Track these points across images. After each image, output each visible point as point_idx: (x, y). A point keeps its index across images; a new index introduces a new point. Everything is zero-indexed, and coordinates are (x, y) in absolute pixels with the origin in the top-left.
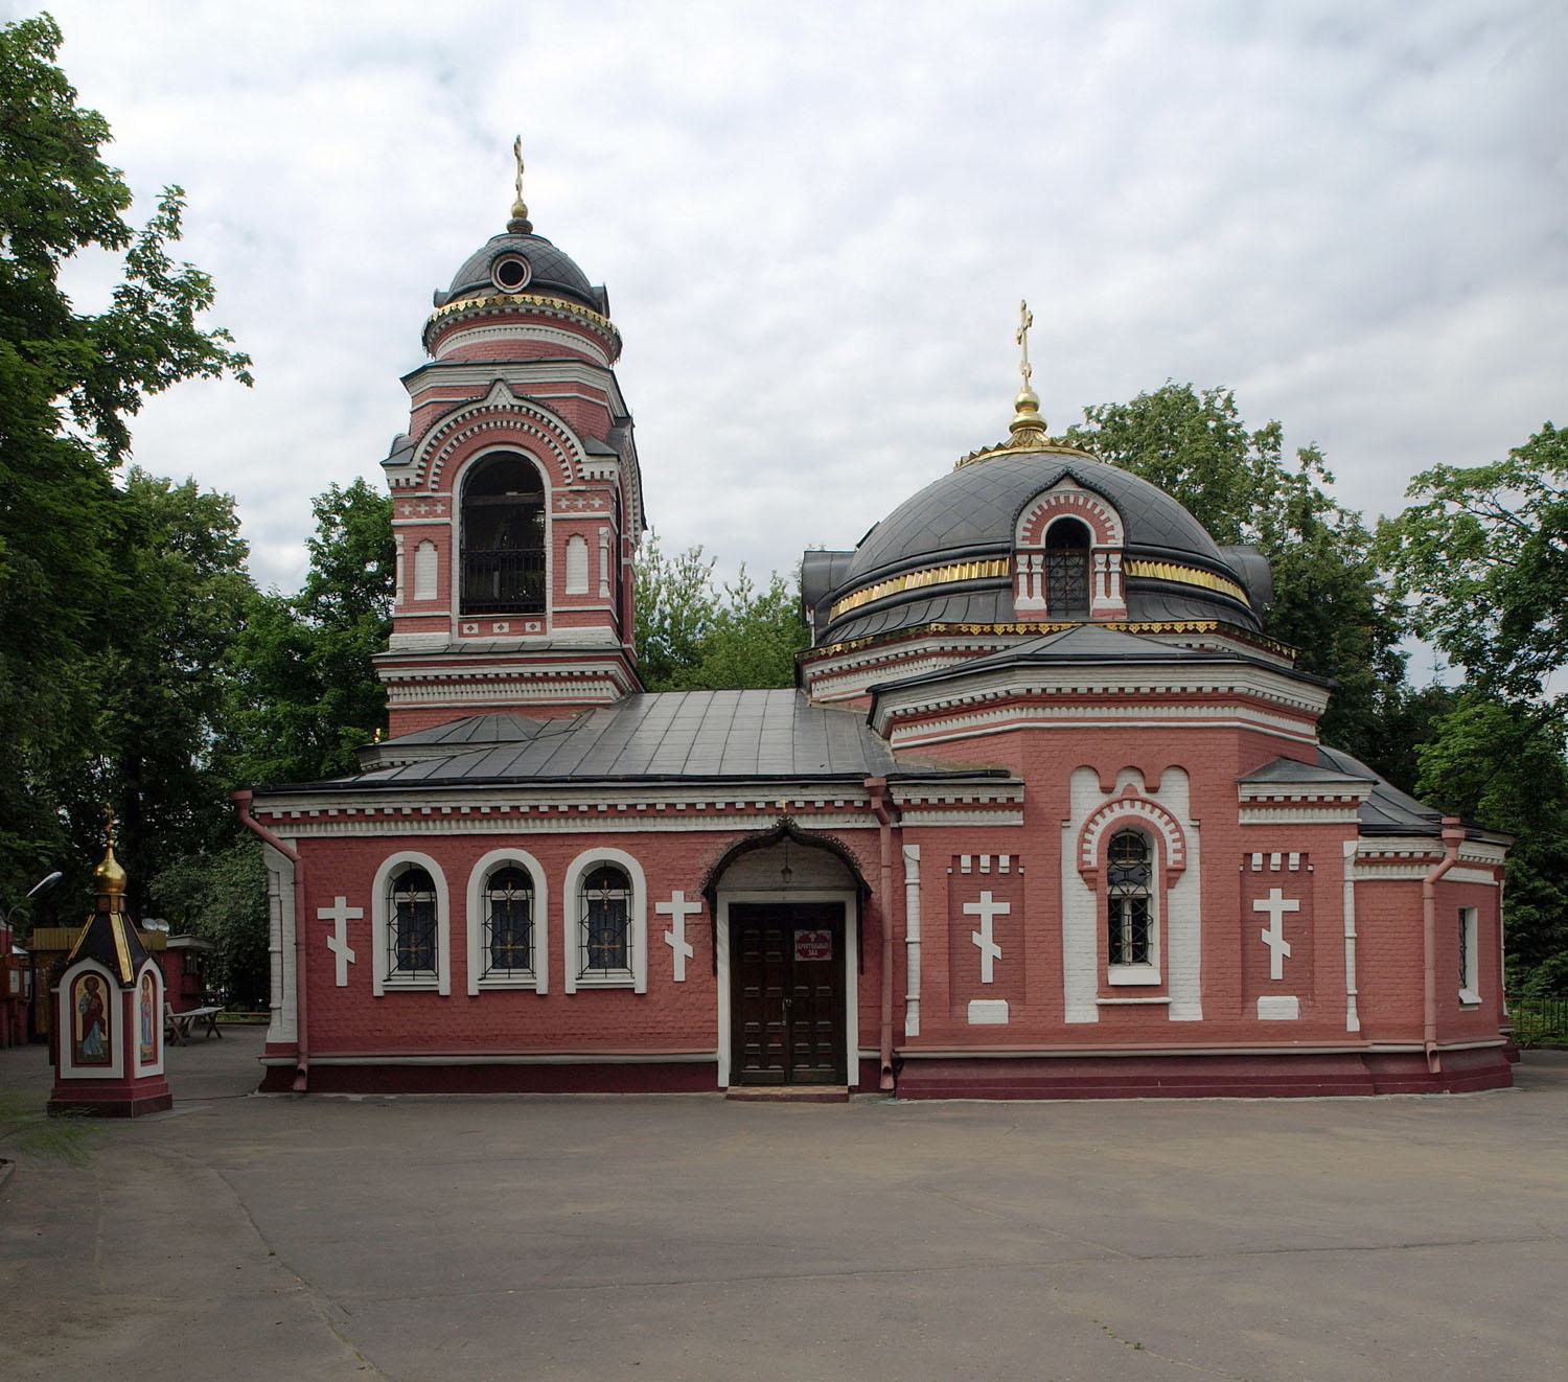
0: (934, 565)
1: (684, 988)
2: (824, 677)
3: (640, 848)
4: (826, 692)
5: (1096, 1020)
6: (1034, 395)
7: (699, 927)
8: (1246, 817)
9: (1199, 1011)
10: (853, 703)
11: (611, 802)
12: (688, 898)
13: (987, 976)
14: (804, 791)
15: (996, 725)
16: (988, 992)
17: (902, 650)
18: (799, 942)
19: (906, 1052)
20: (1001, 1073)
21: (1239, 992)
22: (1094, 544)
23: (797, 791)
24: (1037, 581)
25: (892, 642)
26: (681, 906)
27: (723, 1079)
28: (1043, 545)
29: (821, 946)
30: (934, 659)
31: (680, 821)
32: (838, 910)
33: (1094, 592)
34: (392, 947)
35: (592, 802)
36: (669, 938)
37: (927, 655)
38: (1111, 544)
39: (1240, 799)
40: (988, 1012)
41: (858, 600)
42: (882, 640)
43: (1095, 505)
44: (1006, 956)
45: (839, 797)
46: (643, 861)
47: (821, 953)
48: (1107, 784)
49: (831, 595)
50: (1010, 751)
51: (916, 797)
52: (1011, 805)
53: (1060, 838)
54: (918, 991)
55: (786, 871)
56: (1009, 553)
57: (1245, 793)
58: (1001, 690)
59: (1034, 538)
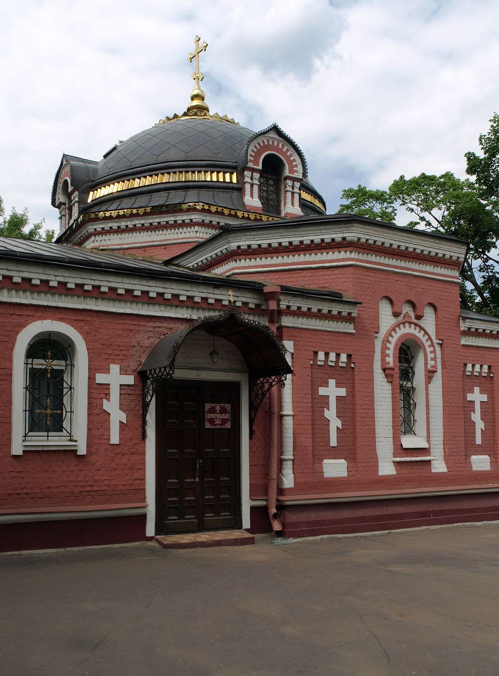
0: (185, 169)
1: (119, 450)
2: (96, 233)
3: (83, 324)
4: (103, 243)
5: (394, 473)
6: (202, 91)
7: (131, 397)
8: (464, 341)
9: (444, 465)
10: (129, 251)
11: (62, 279)
12: (124, 371)
13: (333, 442)
14: (217, 291)
15: (330, 261)
16: (335, 453)
17: (173, 219)
18: (207, 413)
19: (289, 500)
20: (346, 514)
21: (463, 453)
22: (287, 173)
23: (211, 290)
24: (256, 188)
25: (167, 212)
26: (116, 378)
27: (150, 530)
28: (260, 167)
29: (212, 416)
30: (196, 228)
31: (117, 304)
32: (236, 386)
33: (285, 203)
34: (69, 414)
35: (44, 277)
36: (106, 405)
37: (192, 224)
38: (295, 175)
39: (462, 329)
40: (335, 468)
41: (103, 192)
42: (157, 210)
43: (288, 150)
44: (344, 427)
45: (240, 299)
46: (86, 335)
47: (224, 421)
48: (397, 310)
49: (90, 183)
50: (342, 280)
51: (295, 303)
52: (349, 319)
53: (374, 344)
54: (292, 453)
55: (212, 354)
56: (239, 169)
57: (463, 326)
58: (338, 237)
59: (256, 162)
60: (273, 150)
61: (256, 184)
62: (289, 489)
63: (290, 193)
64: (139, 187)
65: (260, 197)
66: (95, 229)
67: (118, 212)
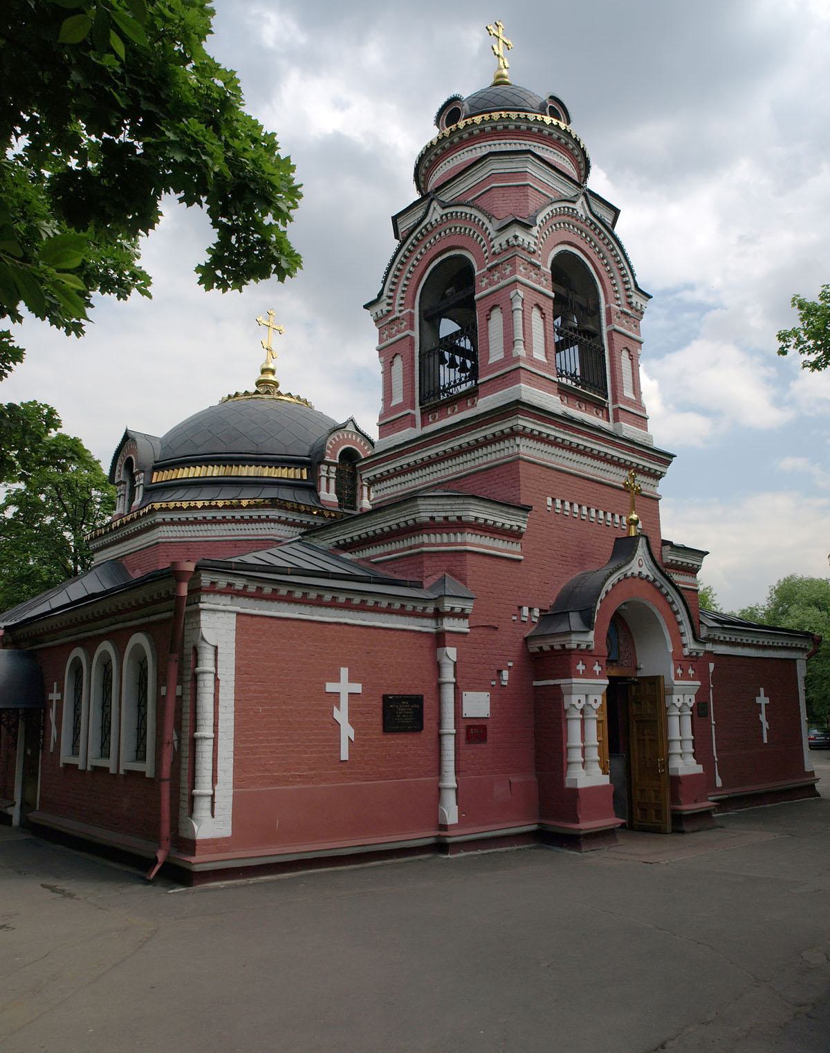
24: (332, 482)
28: (338, 462)
60: (346, 444)
61: (333, 478)
62: (506, 670)
63: (326, 479)
64: (199, 477)
65: (337, 493)
66: (164, 519)
67: (189, 504)
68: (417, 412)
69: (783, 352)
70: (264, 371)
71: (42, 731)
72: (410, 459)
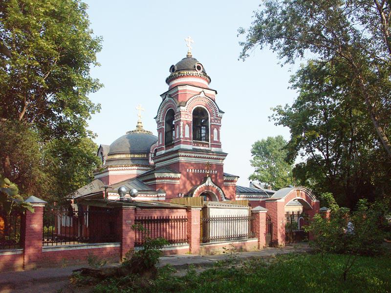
68: (164, 147)
69: (269, 121)
70: (138, 123)
71: (203, 131)
72: (162, 159)
